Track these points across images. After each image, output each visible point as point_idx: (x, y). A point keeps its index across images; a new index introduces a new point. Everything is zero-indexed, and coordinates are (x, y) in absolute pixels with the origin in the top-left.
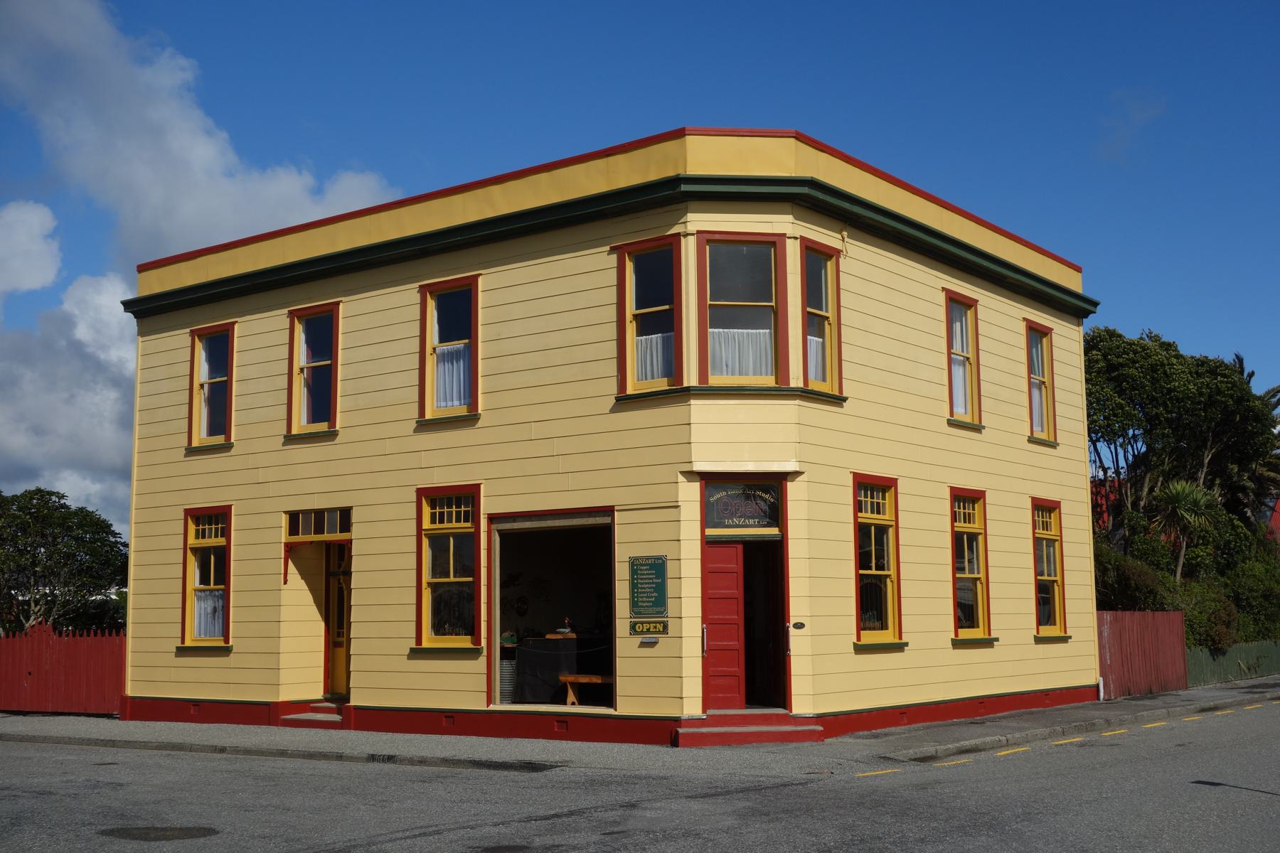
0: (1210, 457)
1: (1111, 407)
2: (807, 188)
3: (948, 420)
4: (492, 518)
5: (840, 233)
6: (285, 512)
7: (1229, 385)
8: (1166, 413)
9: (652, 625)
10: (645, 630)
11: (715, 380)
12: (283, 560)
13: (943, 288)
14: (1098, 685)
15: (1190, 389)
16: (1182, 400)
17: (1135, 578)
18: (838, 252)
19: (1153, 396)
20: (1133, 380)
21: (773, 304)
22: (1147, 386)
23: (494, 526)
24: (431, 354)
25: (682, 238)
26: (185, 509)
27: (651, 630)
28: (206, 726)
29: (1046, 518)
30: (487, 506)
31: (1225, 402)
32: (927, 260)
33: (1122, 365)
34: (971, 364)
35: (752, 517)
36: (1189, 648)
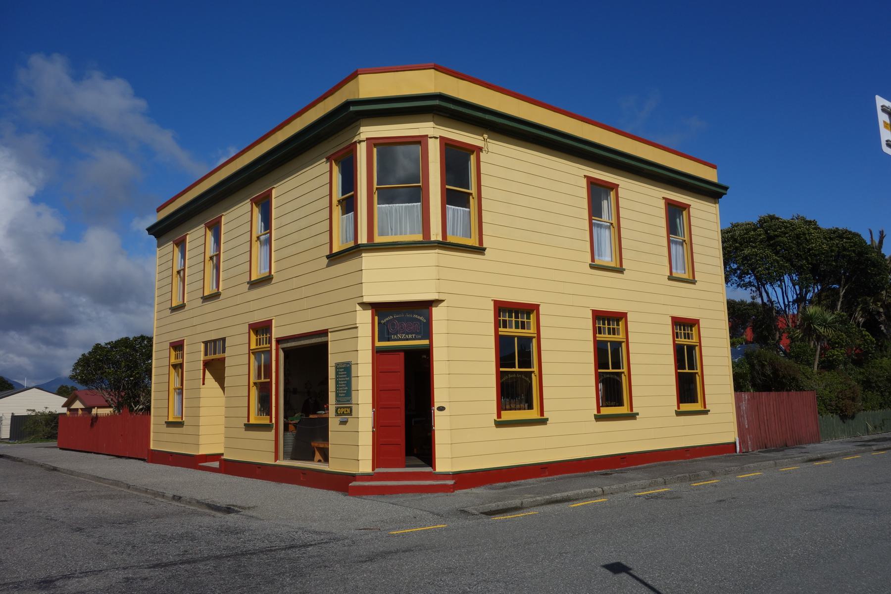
0: (844, 291)
1: (770, 262)
2: (438, 101)
3: (590, 264)
4: (279, 341)
5: (482, 135)
6: (203, 342)
7: (852, 244)
8: (807, 264)
9: (345, 409)
10: (342, 413)
11: (378, 239)
12: (202, 371)
13: (584, 175)
14: (735, 442)
15: (823, 248)
16: (818, 255)
17: (782, 370)
18: (480, 149)
19: (798, 254)
20: (784, 244)
21: (420, 184)
22: (793, 247)
23: (281, 346)
24: (256, 241)
25: (358, 144)
26: (170, 343)
27: (345, 413)
28: (174, 468)
29: (688, 331)
30: (276, 333)
31: (849, 255)
32: (506, 138)
33: (777, 236)
34: (614, 227)
35: (412, 333)
36: (822, 415)
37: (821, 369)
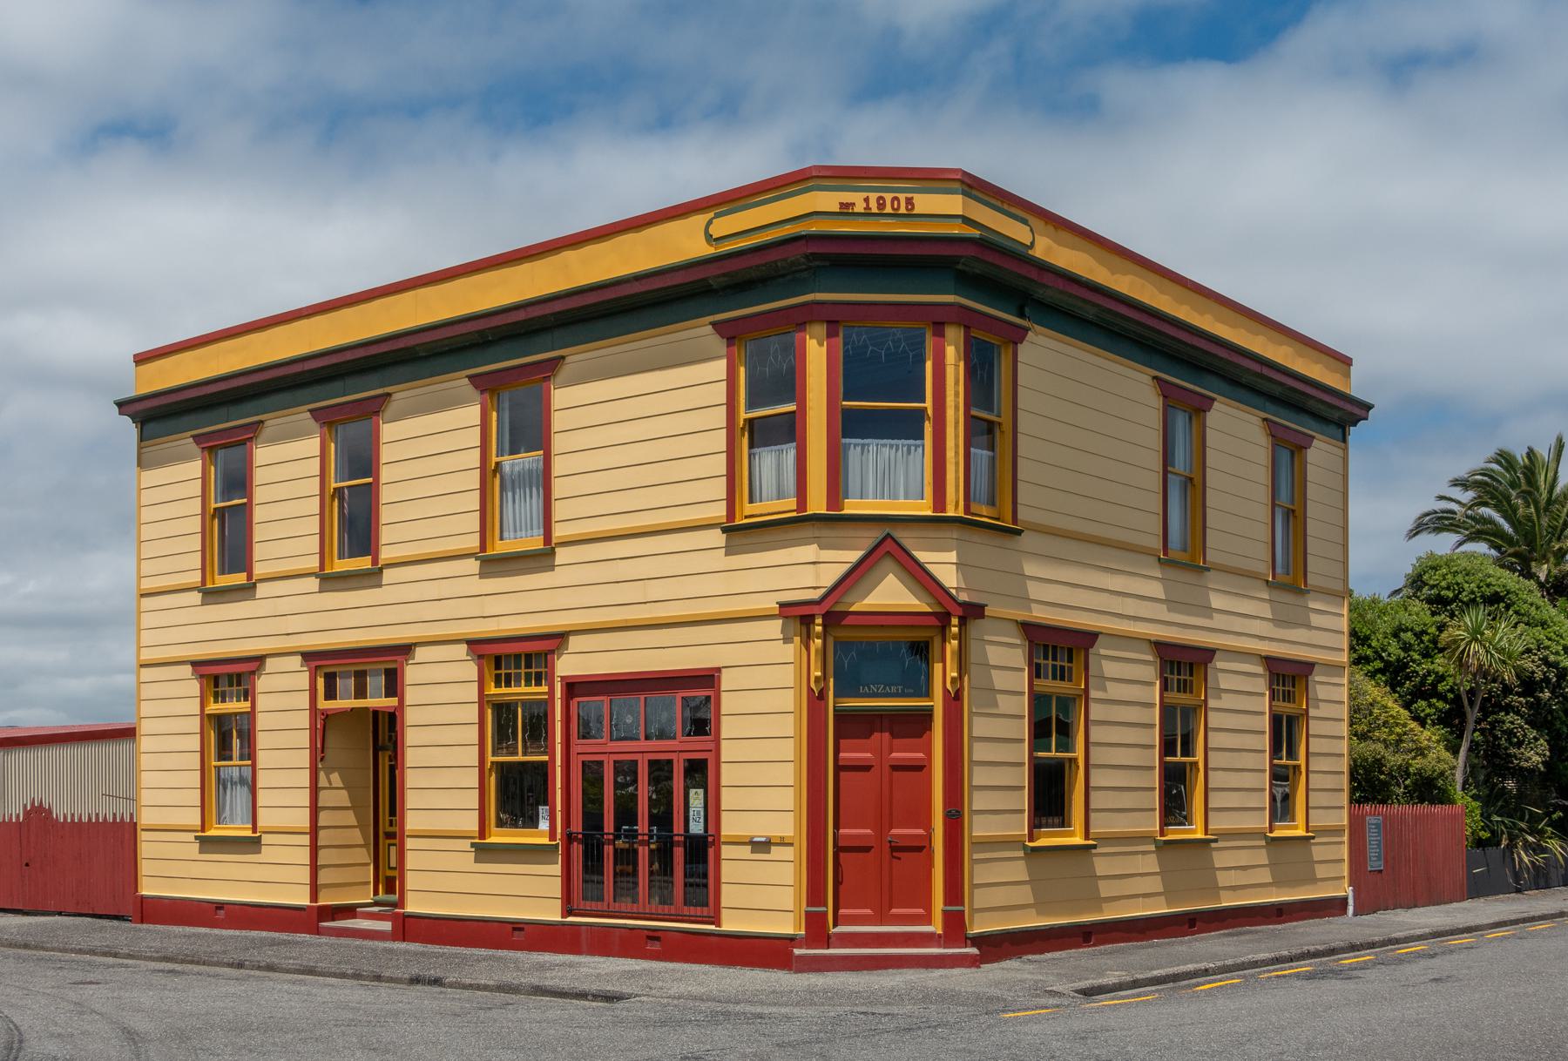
37: (1359, 801)
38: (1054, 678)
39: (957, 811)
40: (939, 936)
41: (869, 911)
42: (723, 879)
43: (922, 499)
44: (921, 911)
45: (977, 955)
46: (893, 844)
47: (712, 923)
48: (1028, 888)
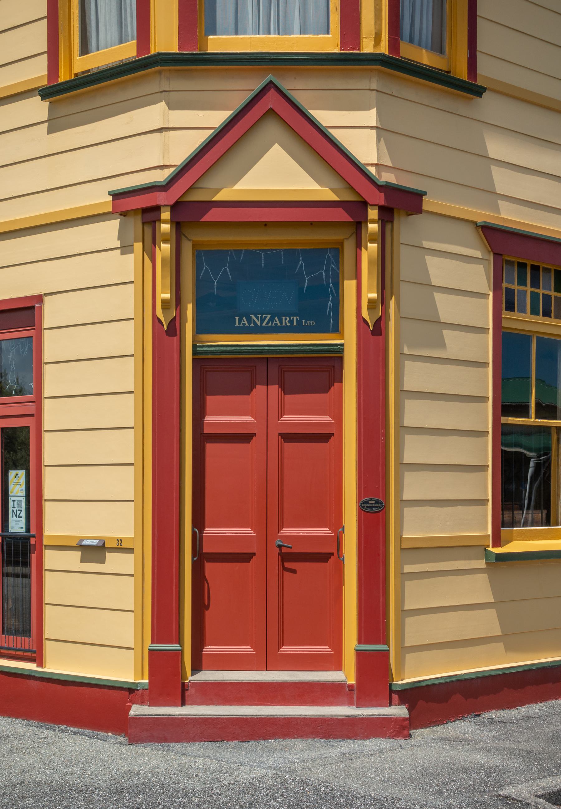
38: (534, 312)
39: (377, 502)
40: (351, 687)
41: (247, 649)
42: (47, 599)
43: (328, 33)
44: (325, 649)
45: (405, 719)
46: (284, 550)
47: (32, 660)
48: (492, 613)
